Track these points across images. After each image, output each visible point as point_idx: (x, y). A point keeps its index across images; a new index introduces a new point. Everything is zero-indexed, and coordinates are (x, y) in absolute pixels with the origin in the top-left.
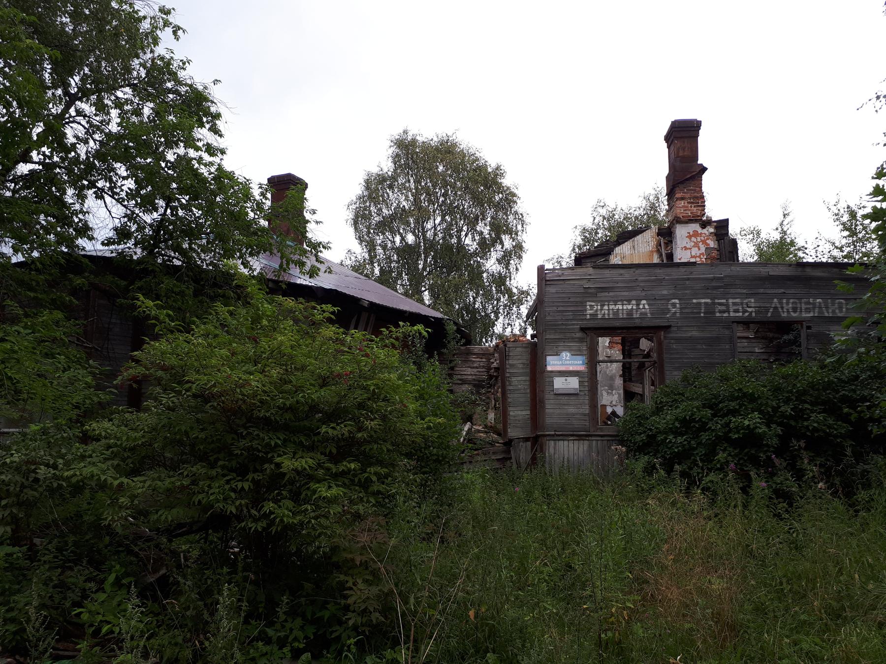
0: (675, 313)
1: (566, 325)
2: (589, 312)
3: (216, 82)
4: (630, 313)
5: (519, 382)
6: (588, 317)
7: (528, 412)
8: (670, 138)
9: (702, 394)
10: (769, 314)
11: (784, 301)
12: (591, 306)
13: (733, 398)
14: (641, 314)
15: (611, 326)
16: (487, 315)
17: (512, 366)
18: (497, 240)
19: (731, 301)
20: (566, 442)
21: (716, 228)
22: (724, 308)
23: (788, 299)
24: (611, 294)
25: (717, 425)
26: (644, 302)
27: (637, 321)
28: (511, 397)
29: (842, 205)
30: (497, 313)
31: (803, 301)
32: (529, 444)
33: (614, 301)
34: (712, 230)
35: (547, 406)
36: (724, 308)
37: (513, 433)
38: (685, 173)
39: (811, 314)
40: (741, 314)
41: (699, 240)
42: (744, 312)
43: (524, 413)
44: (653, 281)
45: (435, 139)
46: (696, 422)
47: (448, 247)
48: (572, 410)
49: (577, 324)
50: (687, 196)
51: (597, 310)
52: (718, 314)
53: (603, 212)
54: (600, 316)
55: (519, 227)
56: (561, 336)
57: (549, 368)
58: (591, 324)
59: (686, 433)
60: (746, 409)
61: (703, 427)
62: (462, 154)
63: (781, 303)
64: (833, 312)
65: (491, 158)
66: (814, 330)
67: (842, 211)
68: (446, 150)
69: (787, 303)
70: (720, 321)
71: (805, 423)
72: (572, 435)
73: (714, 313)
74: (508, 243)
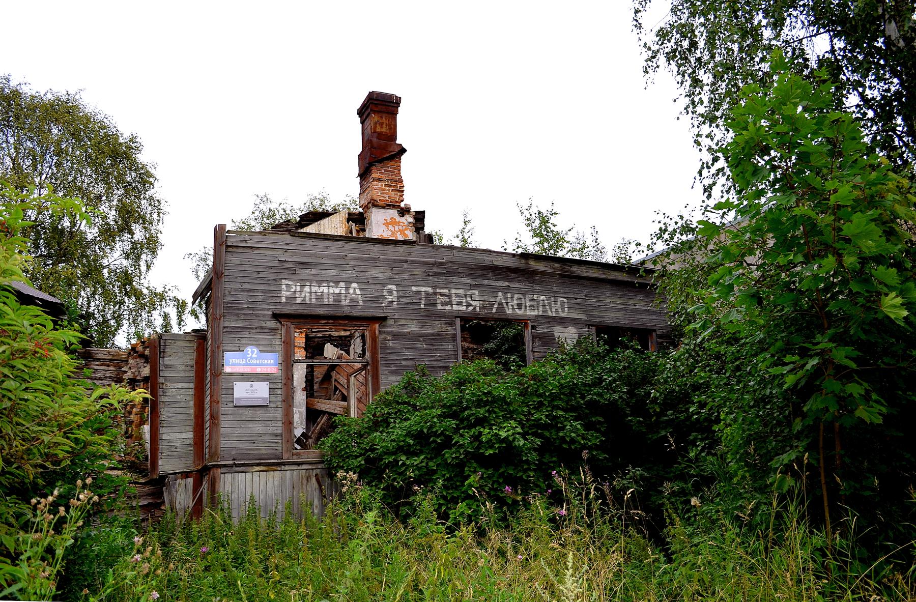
0: (391, 302)
1: (253, 309)
2: (284, 294)
4: (337, 298)
5: (178, 392)
6: (284, 300)
7: (191, 435)
8: (363, 112)
9: (440, 400)
10: (494, 311)
11: (509, 296)
12: (287, 285)
13: (480, 403)
14: (351, 300)
15: (313, 313)
16: (105, 321)
17: (168, 366)
18: (125, 228)
19: (453, 291)
20: (249, 475)
21: (415, 218)
22: (446, 299)
23: (513, 294)
24: (313, 272)
25: (465, 439)
26: (354, 285)
27: (346, 309)
29: (534, 210)
30: (118, 318)
31: (528, 296)
32: (190, 481)
33: (317, 281)
34: (411, 220)
35: (223, 424)
36: (446, 299)
37: (165, 466)
38: (380, 151)
39: (536, 313)
40: (464, 308)
41: (397, 229)
42: (469, 305)
43: (184, 436)
44: (366, 260)
45: (49, 96)
46: (438, 436)
47: (58, 232)
48: (258, 429)
49: (268, 310)
50: (385, 177)
51: (295, 292)
52: (440, 307)
53: (265, 208)
54: (299, 300)
55: (155, 216)
56: (246, 324)
57: (227, 369)
58: (287, 310)
59: (421, 452)
60: (497, 417)
61: (448, 443)
62: (87, 118)
63: (506, 298)
64: (557, 311)
65: (124, 126)
66: (538, 331)
67: (533, 215)
69: (512, 299)
70: (440, 316)
71: (561, 434)
72: (258, 465)
73: (435, 305)
74: (139, 234)
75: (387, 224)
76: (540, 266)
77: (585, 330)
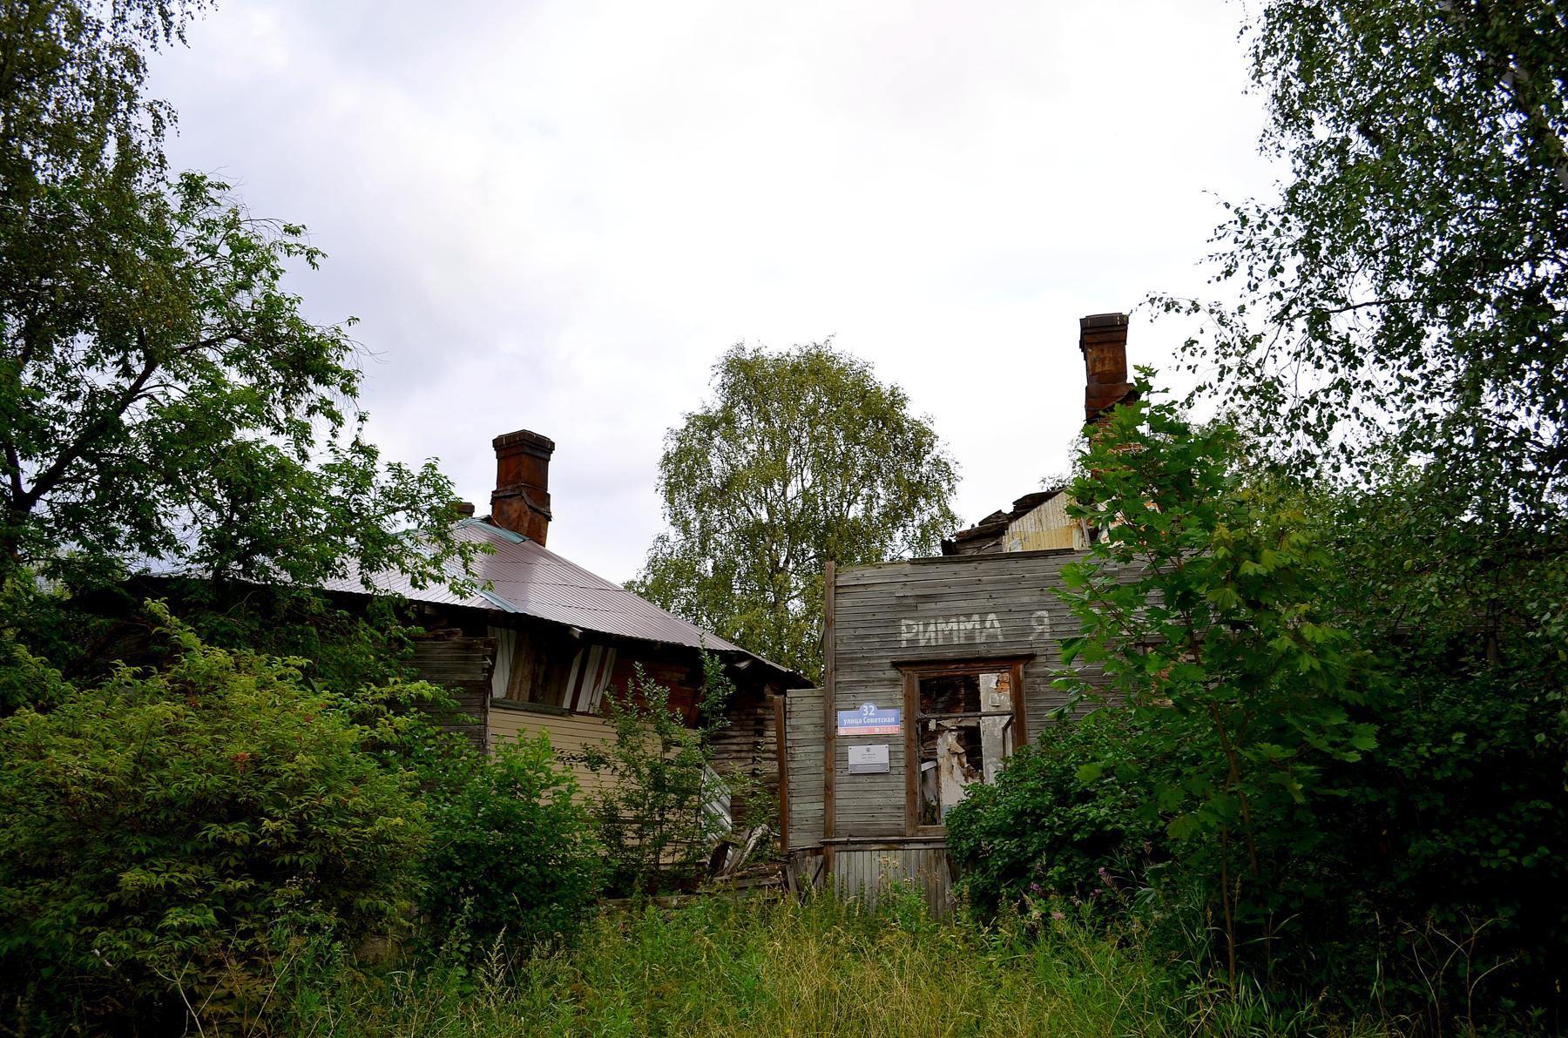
2: (905, 636)
3: (352, 320)
4: (970, 635)
6: (904, 644)
17: (796, 728)
24: (940, 605)
26: (992, 616)
27: (981, 648)
28: (795, 782)
46: (1029, 815)
48: (878, 800)
54: (922, 643)
57: (842, 731)
58: (908, 656)
65: (884, 377)
68: (816, 370)
72: (876, 842)
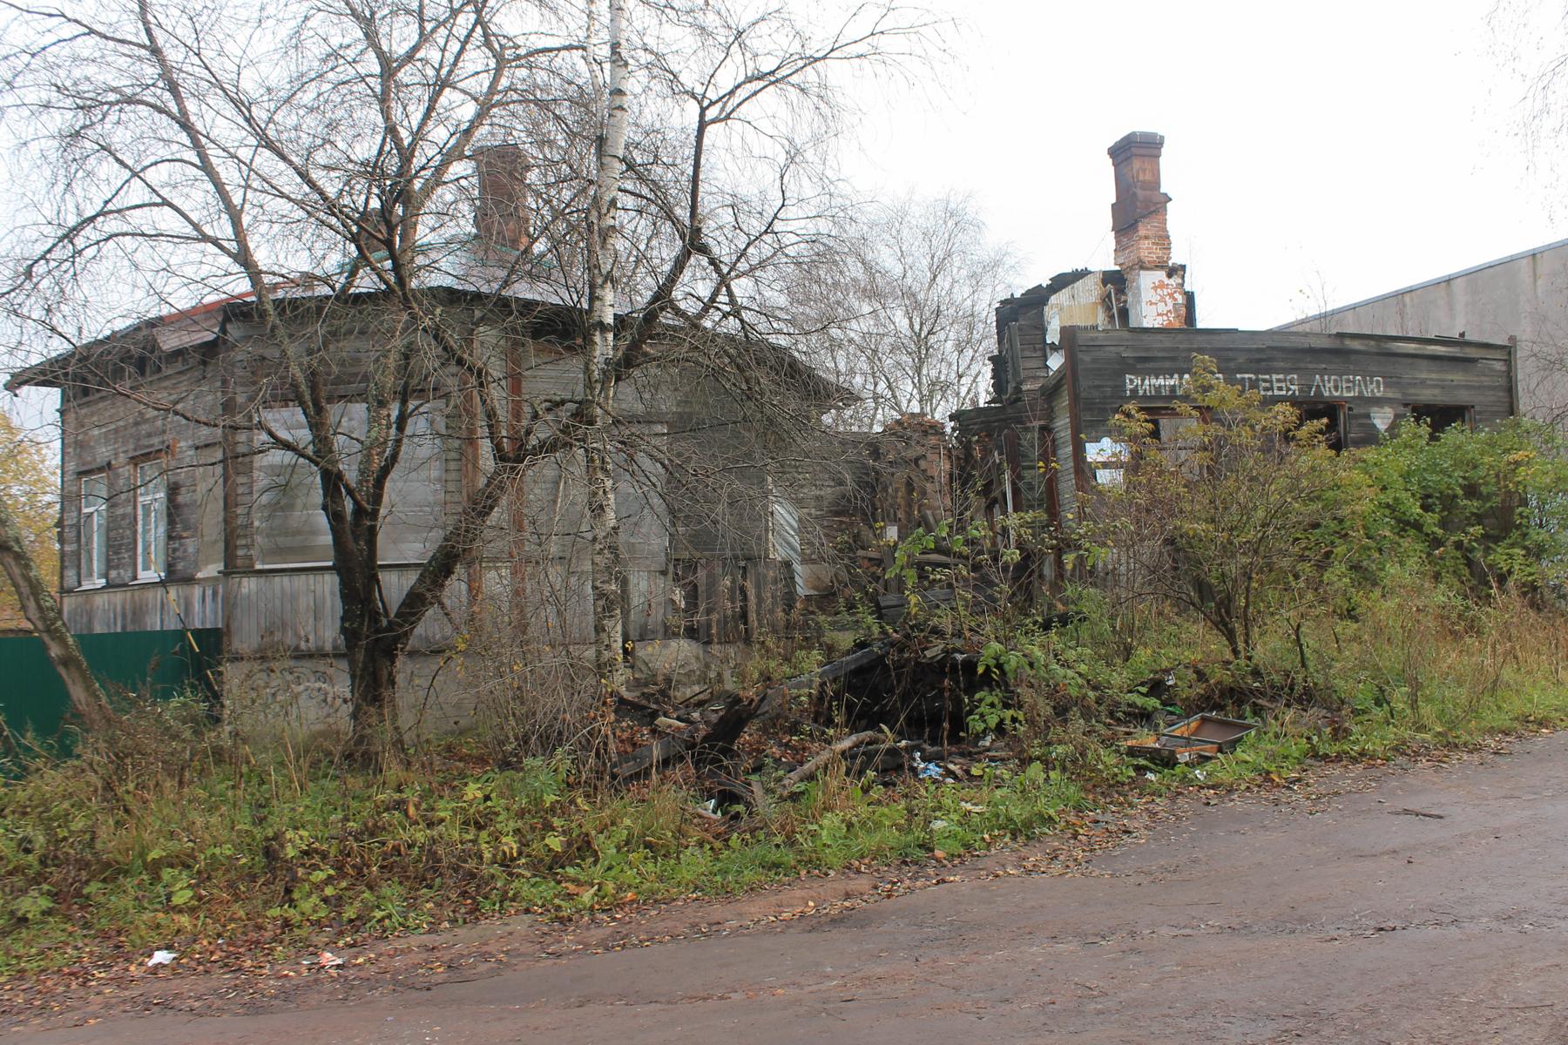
19: (1275, 377)
38: (1138, 207)
75: (1155, 288)
76: (1356, 345)
77: (1401, 410)
